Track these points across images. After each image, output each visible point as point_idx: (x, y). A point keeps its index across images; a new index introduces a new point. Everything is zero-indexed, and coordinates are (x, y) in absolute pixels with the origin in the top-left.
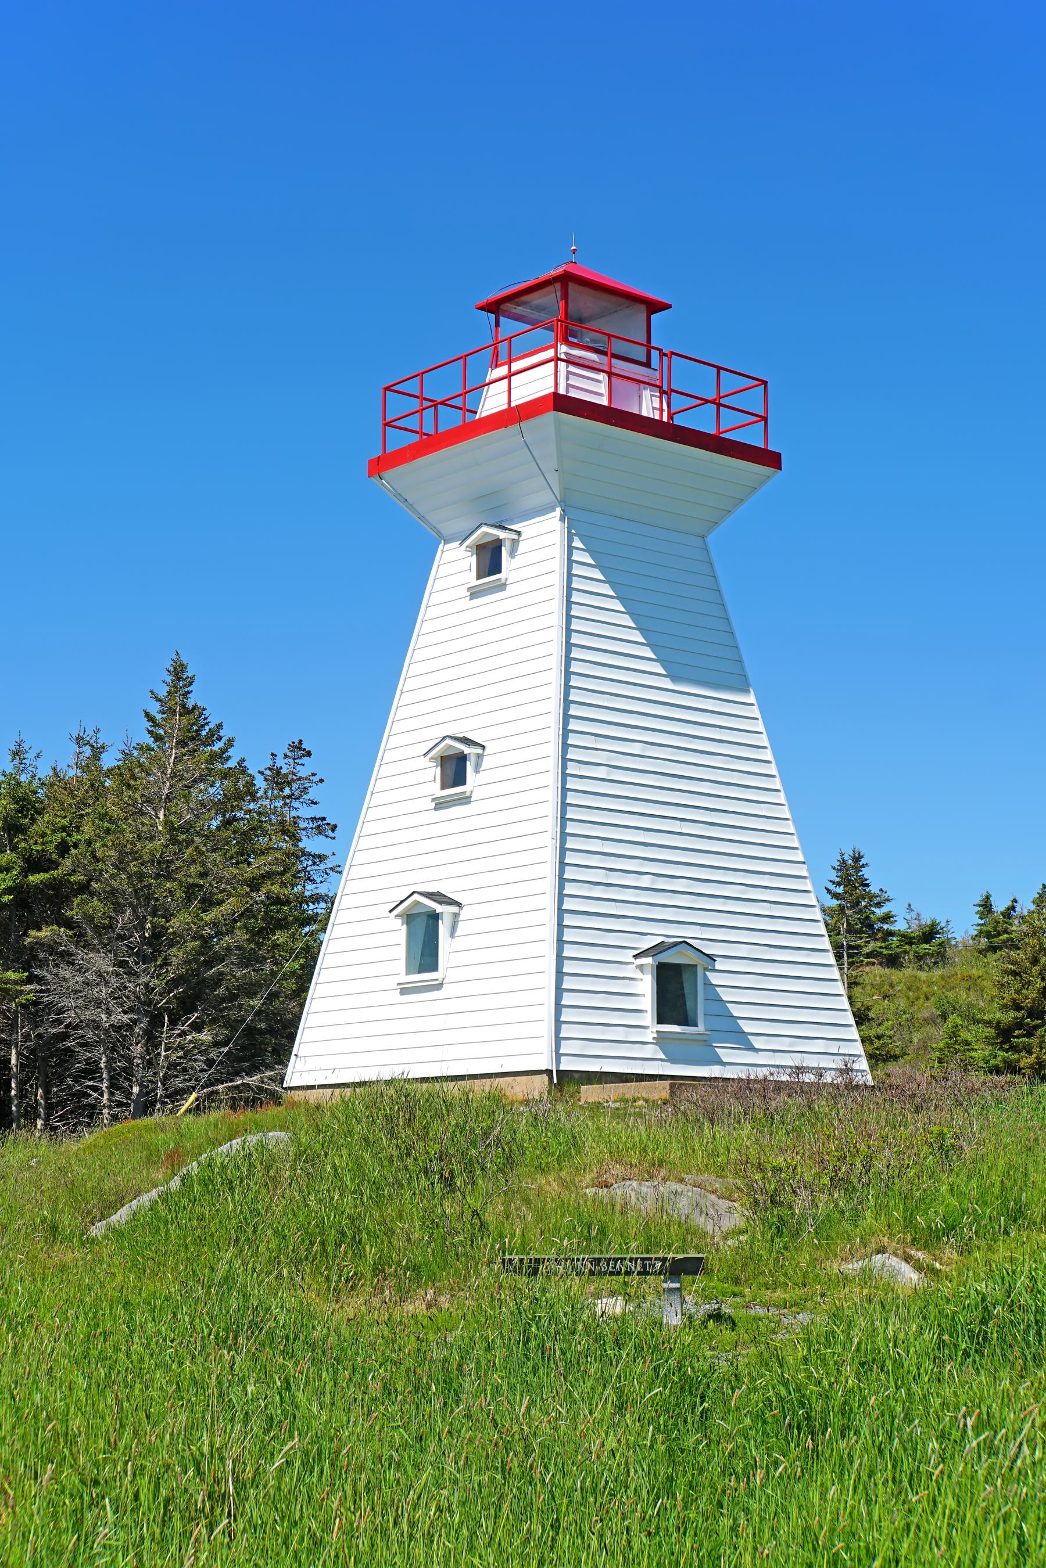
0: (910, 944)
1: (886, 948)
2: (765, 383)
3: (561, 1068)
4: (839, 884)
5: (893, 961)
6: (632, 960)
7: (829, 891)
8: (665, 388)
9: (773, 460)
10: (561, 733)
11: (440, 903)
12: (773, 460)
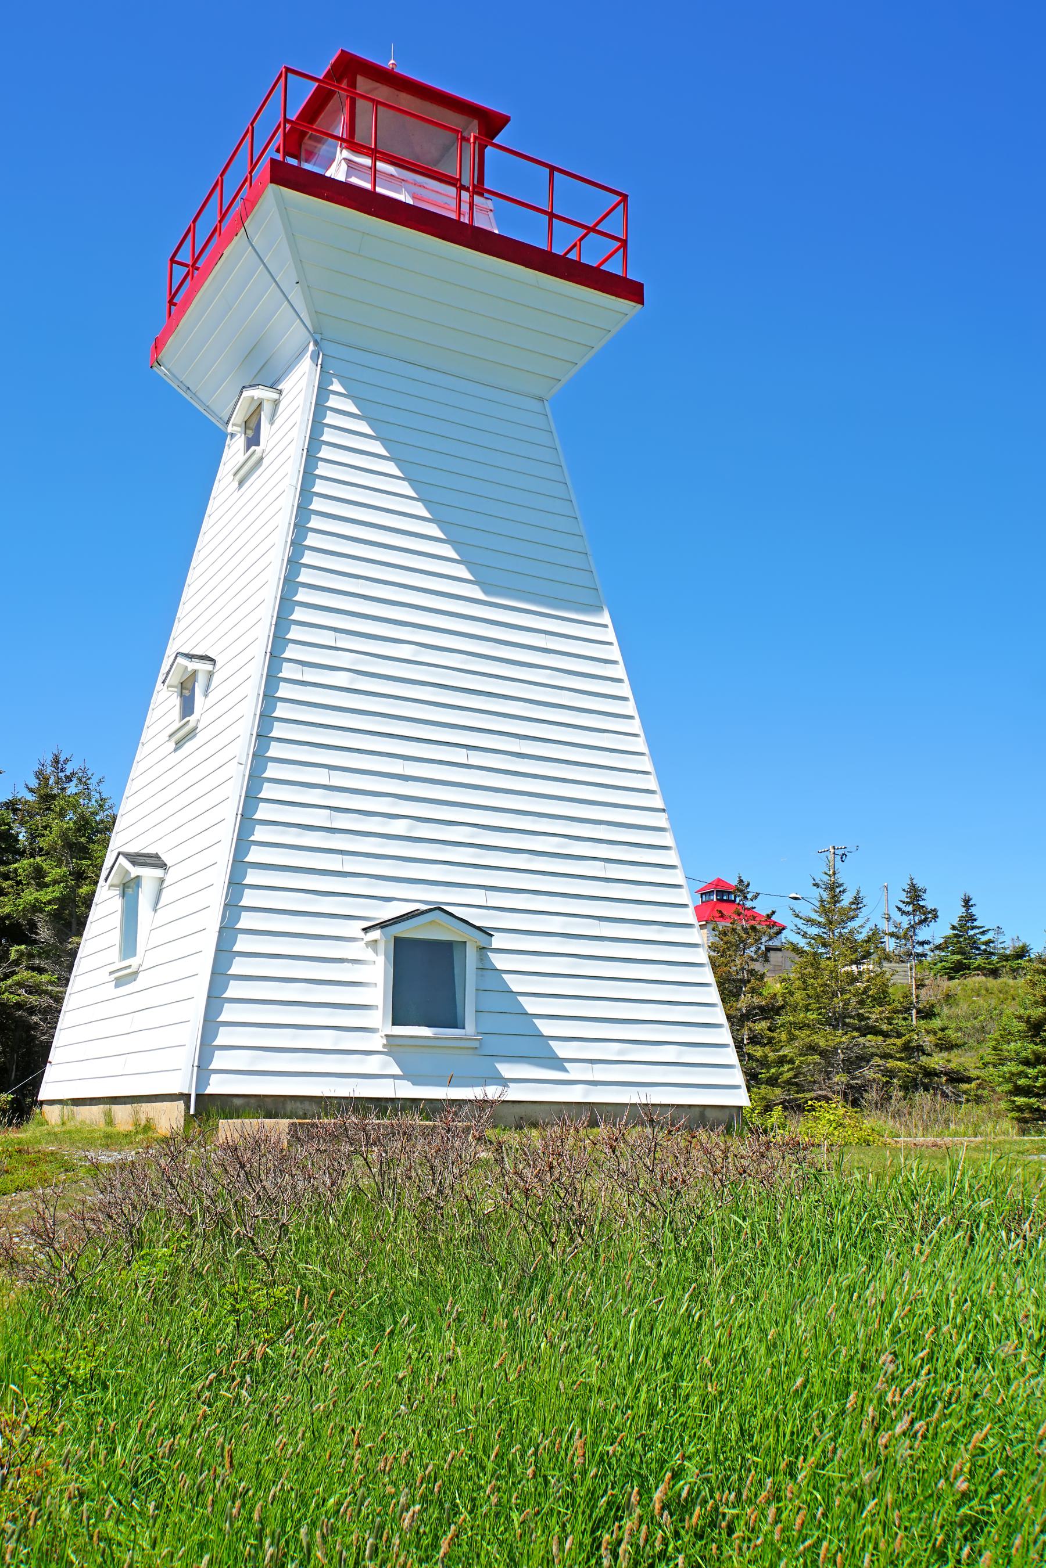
0: (1007, 960)
1: (989, 964)
3: (209, 1091)
4: (908, 903)
5: (994, 973)
6: (362, 934)
7: (899, 909)
9: (632, 291)
10: (274, 622)
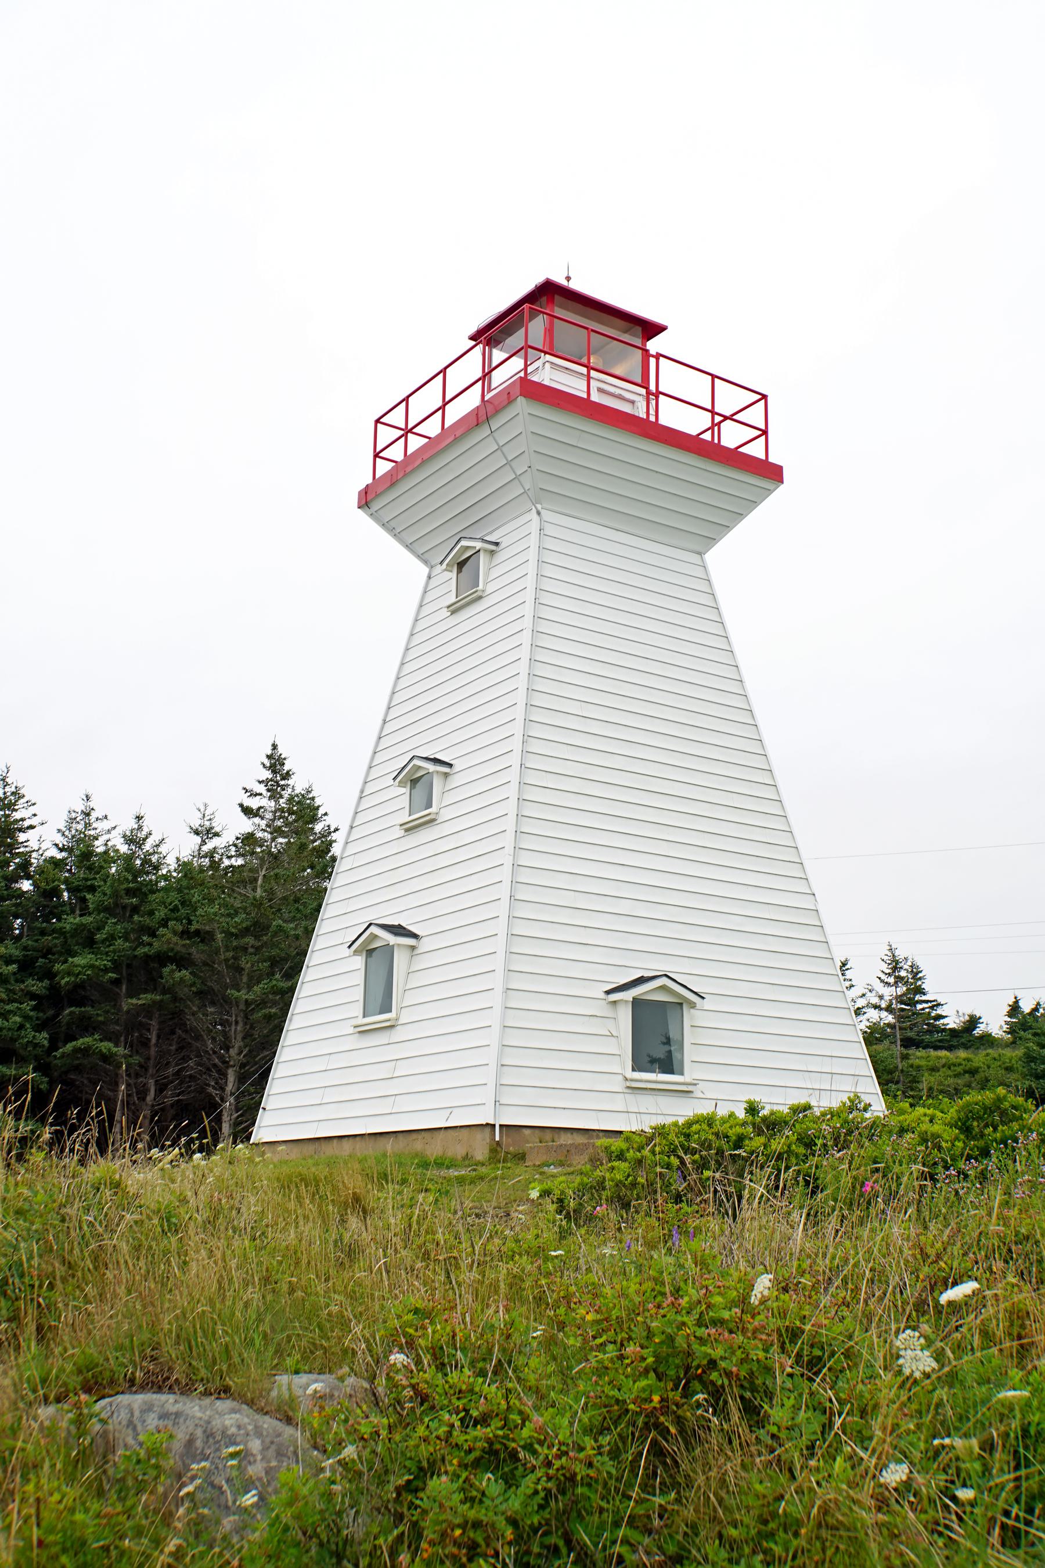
2: (764, 397)
8: (653, 388)
11: (396, 934)
12: (773, 473)
